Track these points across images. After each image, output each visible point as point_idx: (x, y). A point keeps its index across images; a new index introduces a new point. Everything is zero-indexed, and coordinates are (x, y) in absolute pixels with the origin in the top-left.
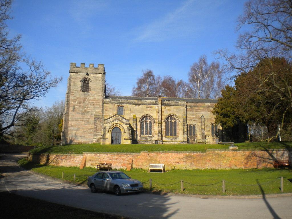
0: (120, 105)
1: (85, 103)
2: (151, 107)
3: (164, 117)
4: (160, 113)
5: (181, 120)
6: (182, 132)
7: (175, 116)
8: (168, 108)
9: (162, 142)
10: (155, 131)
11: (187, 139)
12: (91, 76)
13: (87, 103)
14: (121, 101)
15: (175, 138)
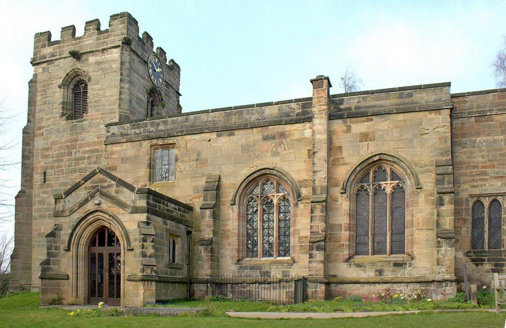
0: (160, 142)
1: (73, 156)
2: (282, 135)
3: (342, 173)
4: (322, 153)
5: (428, 182)
6: (432, 235)
7: (397, 160)
8: (360, 127)
9: (328, 284)
10: (300, 238)
11: (452, 270)
12: (89, 66)
13: (79, 155)
14: (161, 127)
15: (397, 265)
